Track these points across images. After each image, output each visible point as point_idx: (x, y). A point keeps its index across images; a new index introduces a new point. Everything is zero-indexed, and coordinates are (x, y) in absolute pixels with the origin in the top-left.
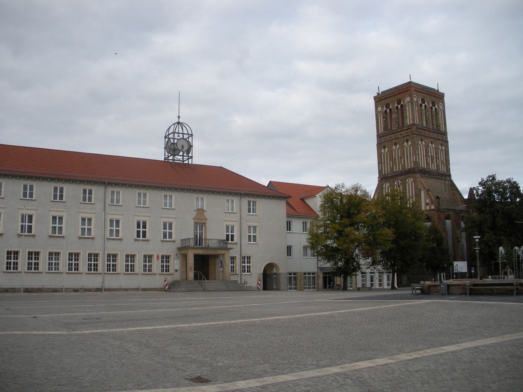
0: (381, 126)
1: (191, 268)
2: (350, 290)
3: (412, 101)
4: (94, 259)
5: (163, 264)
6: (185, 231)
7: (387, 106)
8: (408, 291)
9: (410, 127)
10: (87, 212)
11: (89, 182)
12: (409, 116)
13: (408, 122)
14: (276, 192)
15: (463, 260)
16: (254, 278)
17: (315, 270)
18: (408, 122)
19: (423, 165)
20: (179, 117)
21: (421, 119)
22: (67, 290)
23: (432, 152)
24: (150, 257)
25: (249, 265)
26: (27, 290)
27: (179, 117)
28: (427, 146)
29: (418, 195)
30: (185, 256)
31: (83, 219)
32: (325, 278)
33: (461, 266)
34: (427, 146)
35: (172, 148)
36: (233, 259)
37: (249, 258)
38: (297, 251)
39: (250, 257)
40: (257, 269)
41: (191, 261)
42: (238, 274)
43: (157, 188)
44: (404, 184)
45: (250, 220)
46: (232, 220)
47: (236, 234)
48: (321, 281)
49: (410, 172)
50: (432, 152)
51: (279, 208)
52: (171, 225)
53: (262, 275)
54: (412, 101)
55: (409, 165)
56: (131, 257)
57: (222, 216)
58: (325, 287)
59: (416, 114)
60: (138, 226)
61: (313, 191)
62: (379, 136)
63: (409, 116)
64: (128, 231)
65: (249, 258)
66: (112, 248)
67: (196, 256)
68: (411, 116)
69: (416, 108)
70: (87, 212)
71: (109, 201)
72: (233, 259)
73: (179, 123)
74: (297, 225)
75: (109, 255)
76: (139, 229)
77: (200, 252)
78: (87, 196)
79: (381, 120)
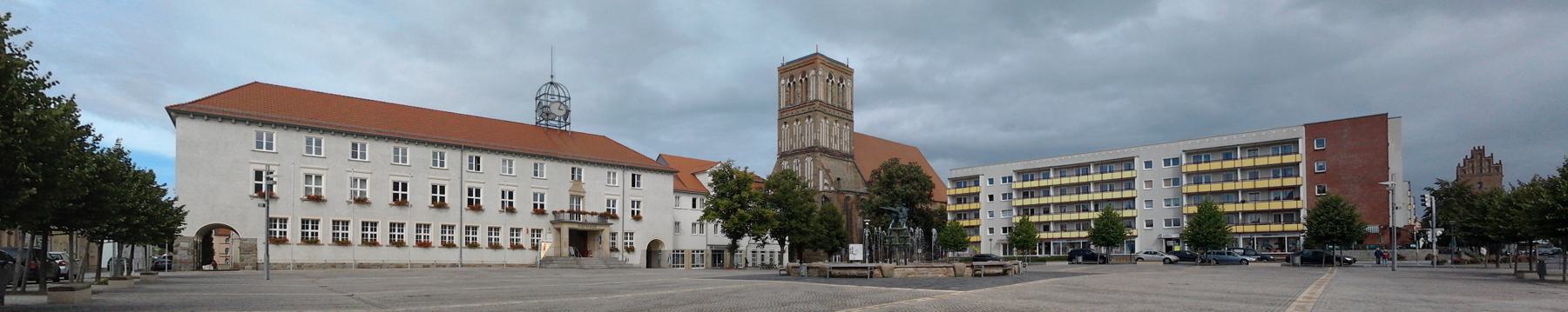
0: (783, 100)
3: (816, 75)
6: (557, 201)
7: (792, 78)
8: (937, 271)
9: (812, 103)
10: (472, 180)
11: (440, 145)
12: (810, 89)
13: (812, 97)
14: (662, 166)
15: (860, 242)
16: (638, 258)
17: (703, 247)
18: (812, 97)
19: (824, 143)
21: (826, 95)
22: (389, 266)
23: (836, 131)
24: (518, 230)
26: (361, 266)
28: (831, 125)
29: (816, 175)
30: (559, 230)
31: (308, 177)
32: (714, 257)
33: (857, 252)
34: (831, 125)
35: (544, 111)
36: (614, 234)
38: (686, 227)
40: (641, 246)
41: (566, 236)
43: (289, 127)
44: (803, 163)
45: (634, 195)
46: (615, 193)
48: (709, 260)
49: (810, 151)
50: (836, 131)
51: (667, 182)
52: (478, 191)
54: (816, 75)
55: (808, 143)
56: (494, 230)
57: (601, 189)
58: (714, 264)
59: (821, 90)
60: (434, 190)
61: (703, 166)
62: (781, 111)
63: (810, 89)
67: (571, 231)
68: (818, 90)
69: (821, 83)
70: (360, 171)
72: (614, 234)
74: (686, 201)
75: (468, 228)
77: (575, 226)
79: (784, 94)
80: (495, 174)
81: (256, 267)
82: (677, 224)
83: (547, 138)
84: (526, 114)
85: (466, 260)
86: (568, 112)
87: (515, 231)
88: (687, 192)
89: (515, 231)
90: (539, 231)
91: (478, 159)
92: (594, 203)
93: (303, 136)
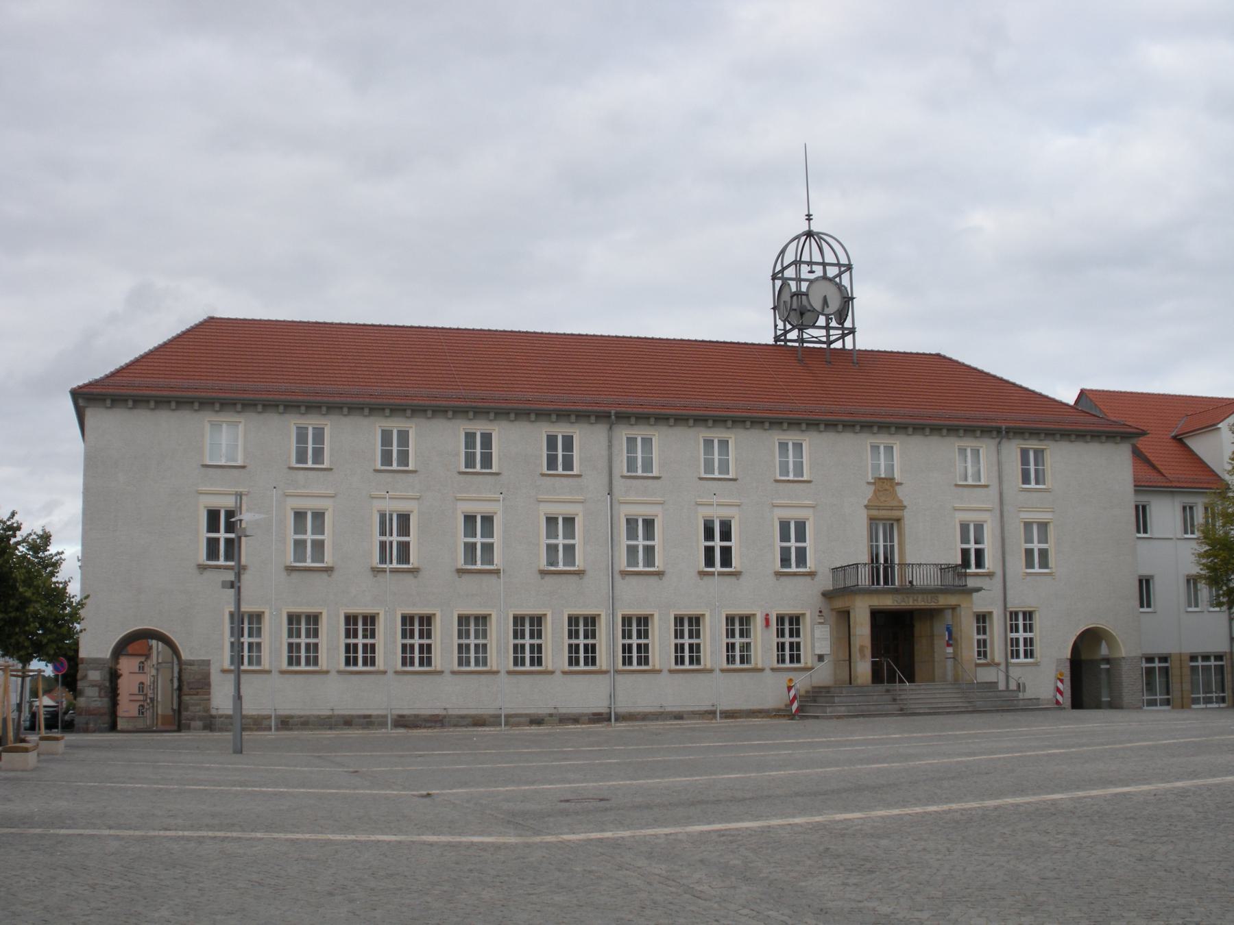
6: (841, 543)
11: (563, 415)
14: (1100, 419)
16: (1045, 675)
20: (809, 218)
24: (746, 620)
25: (1028, 635)
27: (809, 218)
35: (794, 307)
36: (982, 619)
37: (1028, 615)
38: (1169, 591)
42: (998, 664)
45: (1028, 505)
51: (1112, 468)
53: (1068, 664)
57: (947, 496)
64: (679, 549)
65: (1028, 615)
66: (635, 597)
67: (875, 614)
70: (561, 497)
71: (621, 467)
72: (982, 619)
73: (809, 234)
74: (1165, 514)
75: (627, 620)
80: (683, 478)
81: (210, 723)
82: (1145, 584)
83: (810, 378)
84: (755, 324)
85: (624, 704)
86: (847, 300)
87: (739, 624)
88: (1170, 489)
89: (739, 624)
90: (795, 620)
91: (487, 440)
92: (927, 549)
93: (702, 434)
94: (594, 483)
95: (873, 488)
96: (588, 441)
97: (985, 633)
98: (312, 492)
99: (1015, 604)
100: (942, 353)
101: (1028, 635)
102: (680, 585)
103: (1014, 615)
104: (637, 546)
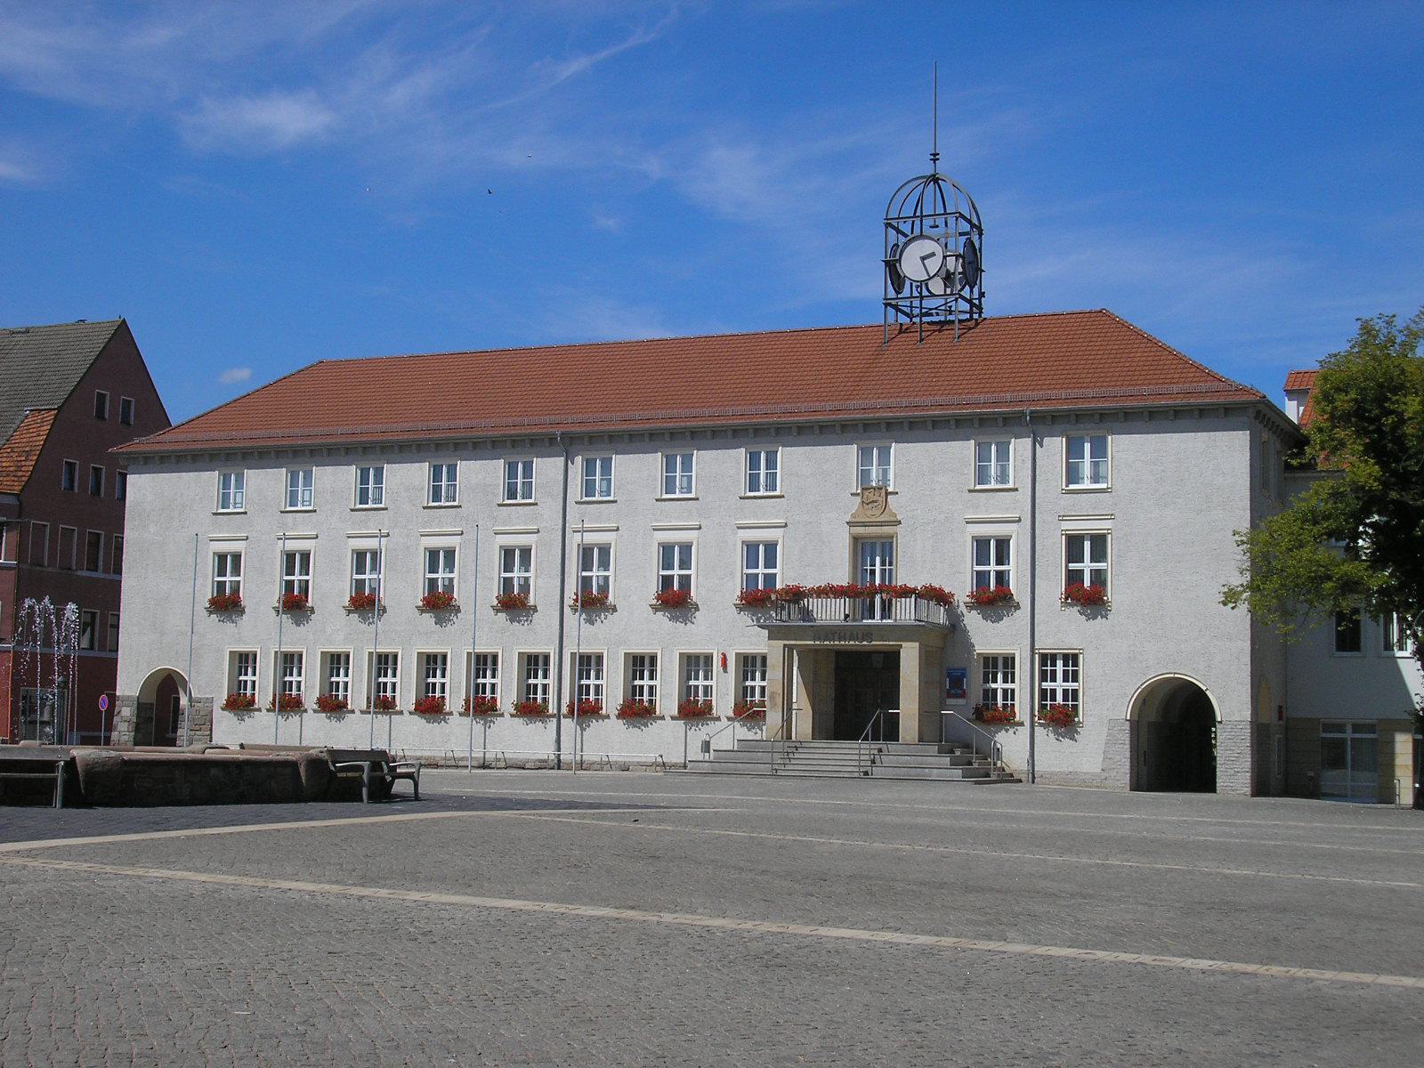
1: (774, 705)
2: (403, 798)
4: (1065, 673)
5: (1009, 686)
20: (935, 157)
25: (1070, 685)
27: (935, 157)
37: (1071, 659)
39: (1075, 657)
42: (1022, 724)
47: (1016, 571)
53: (1127, 726)
64: (633, 584)
65: (1071, 659)
66: (586, 636)
70: (516, 526)
71: (576, 490)
73: (935, 179)
76: (508, 575)
78: (763, 471)
87: (694, 664)
89: (694, 664)
94: (548, 510)
95: (858, 499)
96: (547, 468)
97: (1075, 679)
98: (591, 525)
99: (1046, 643)
100: (1121, 311)
101: (1070, 685)
102: (634, 624)
103: (1048, 659)
104: (765, 575)
